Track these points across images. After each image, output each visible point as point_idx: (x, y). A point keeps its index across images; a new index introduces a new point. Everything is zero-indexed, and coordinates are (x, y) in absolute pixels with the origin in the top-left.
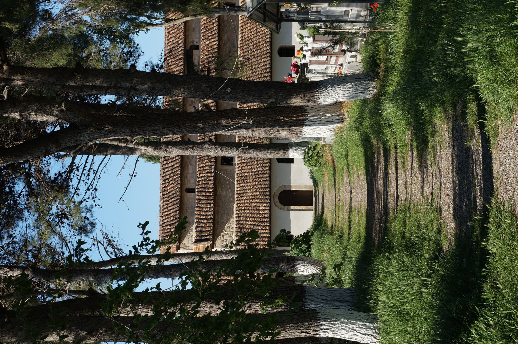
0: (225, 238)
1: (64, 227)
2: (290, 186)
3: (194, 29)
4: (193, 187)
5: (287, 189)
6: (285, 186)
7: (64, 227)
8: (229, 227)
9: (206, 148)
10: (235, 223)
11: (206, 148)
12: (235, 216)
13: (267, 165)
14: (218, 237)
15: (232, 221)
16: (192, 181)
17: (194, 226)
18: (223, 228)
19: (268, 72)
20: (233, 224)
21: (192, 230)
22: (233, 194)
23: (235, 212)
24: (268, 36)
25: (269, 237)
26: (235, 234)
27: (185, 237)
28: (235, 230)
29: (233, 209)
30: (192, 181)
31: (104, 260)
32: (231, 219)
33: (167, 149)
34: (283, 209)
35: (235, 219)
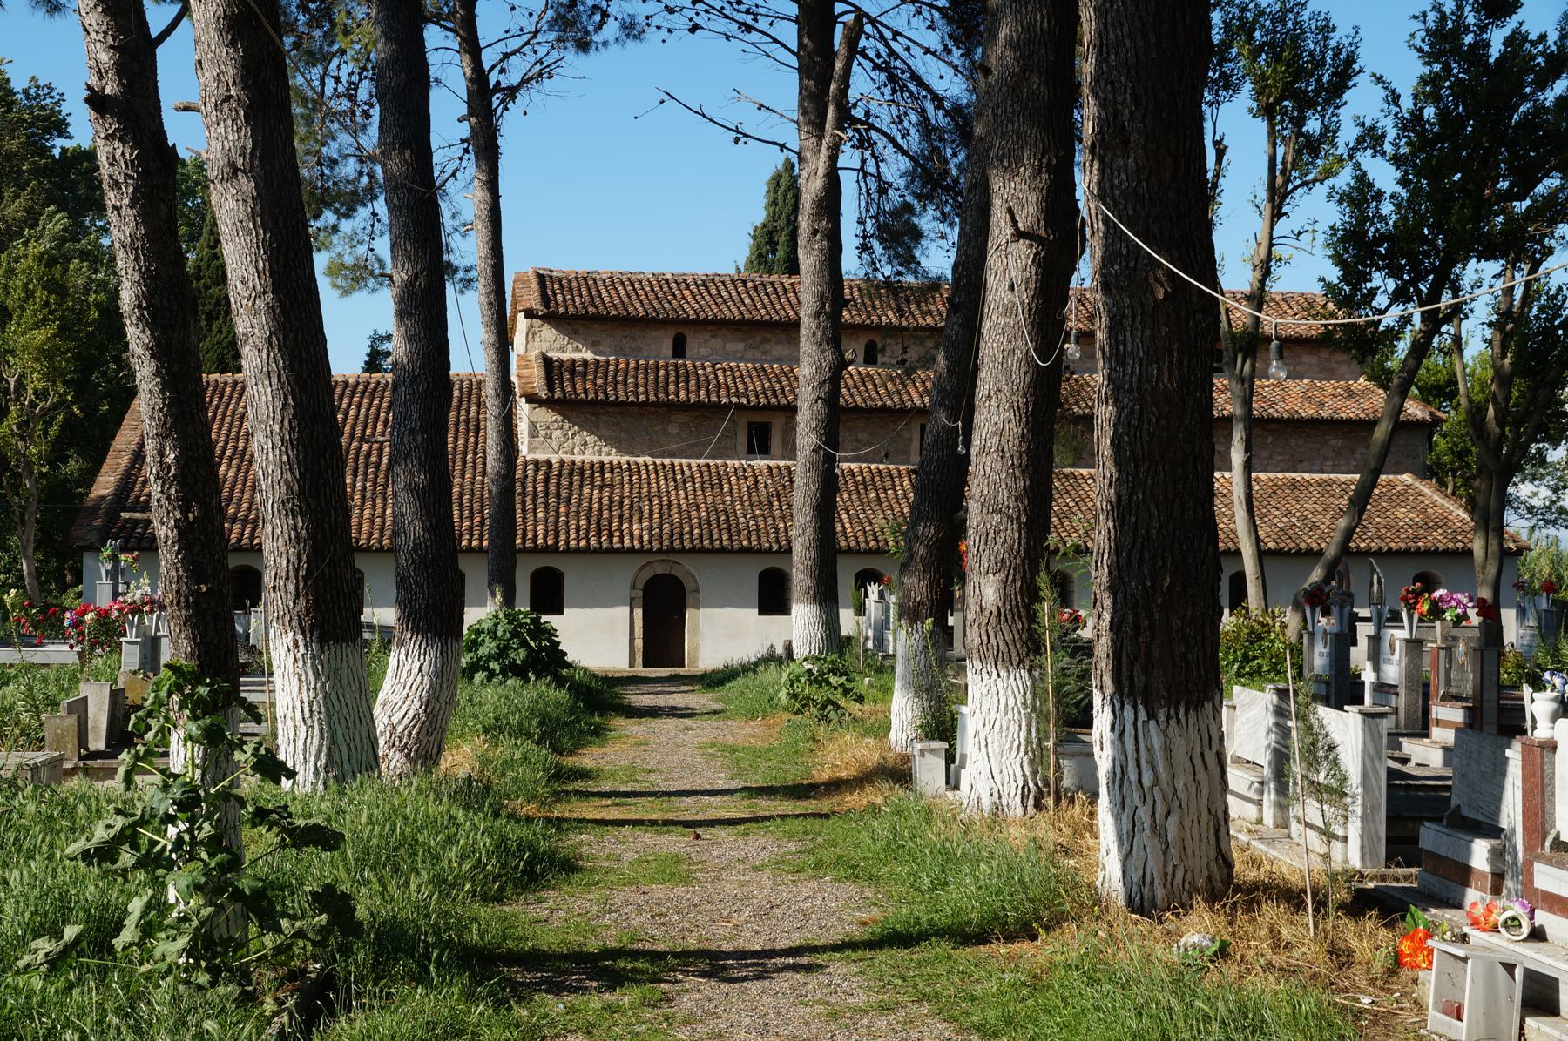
0: (556, 434)
2: (697, 607)
4: (688, 355)
5: (689, 598)
6: (697, 591)
8: (585, 444)
9: (823, 352)
11: (823, 352)
16: (703, 352)
18: (582, 428)
20: (593, 453)
21: (577, 349)
23: (624, 459)
28: (578, 458)
32: (606, 449)
34: (633, 587)
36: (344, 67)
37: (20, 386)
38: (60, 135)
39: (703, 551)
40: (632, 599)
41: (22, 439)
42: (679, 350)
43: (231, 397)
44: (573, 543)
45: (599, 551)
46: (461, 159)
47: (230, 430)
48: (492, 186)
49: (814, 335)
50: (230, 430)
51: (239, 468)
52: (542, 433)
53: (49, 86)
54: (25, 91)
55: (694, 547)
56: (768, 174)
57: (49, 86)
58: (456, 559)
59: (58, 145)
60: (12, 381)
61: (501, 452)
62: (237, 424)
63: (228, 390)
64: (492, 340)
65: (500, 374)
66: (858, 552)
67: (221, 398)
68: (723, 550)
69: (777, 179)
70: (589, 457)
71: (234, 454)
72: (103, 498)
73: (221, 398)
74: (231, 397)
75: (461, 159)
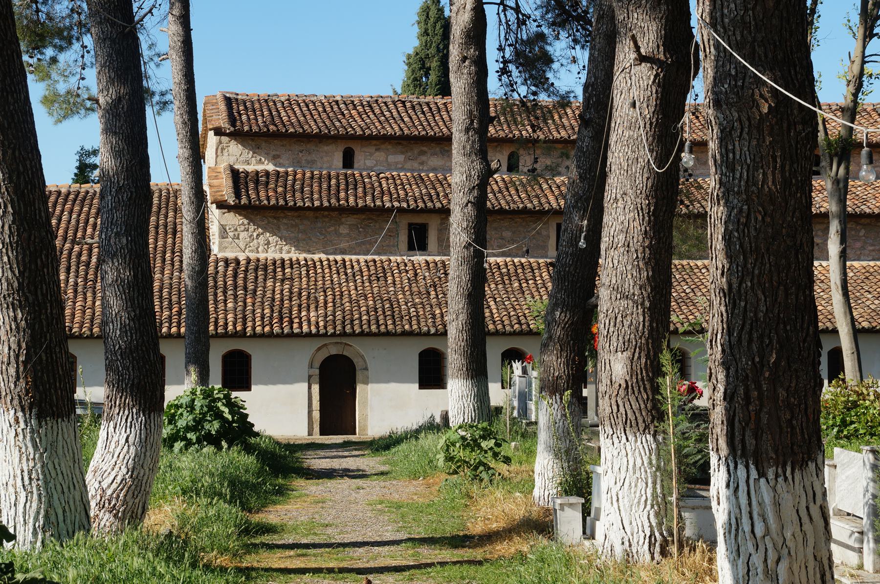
0: (243, 235)
2: (366, 382)
4: (356, 165)
5: (359, 375)
6: (366, 369)
8: (268, 243)
9: (472, 162)
11: (472, 162)
12: (294, 255)
14: (246, 217)
18: (265, 229)
20: (275, 251)
23: (302, 256)
25: (246, 333)
28: (262, 256)
32: (286, 248)
33: (467, 63)
34: (311, 366)
39: (370, 334)
40: (310, 377)
49: (464, 148)
52: (231, 234)
55: (363, 331)
64: (186, 155)
65: (193, 184)
70: (272, 254)
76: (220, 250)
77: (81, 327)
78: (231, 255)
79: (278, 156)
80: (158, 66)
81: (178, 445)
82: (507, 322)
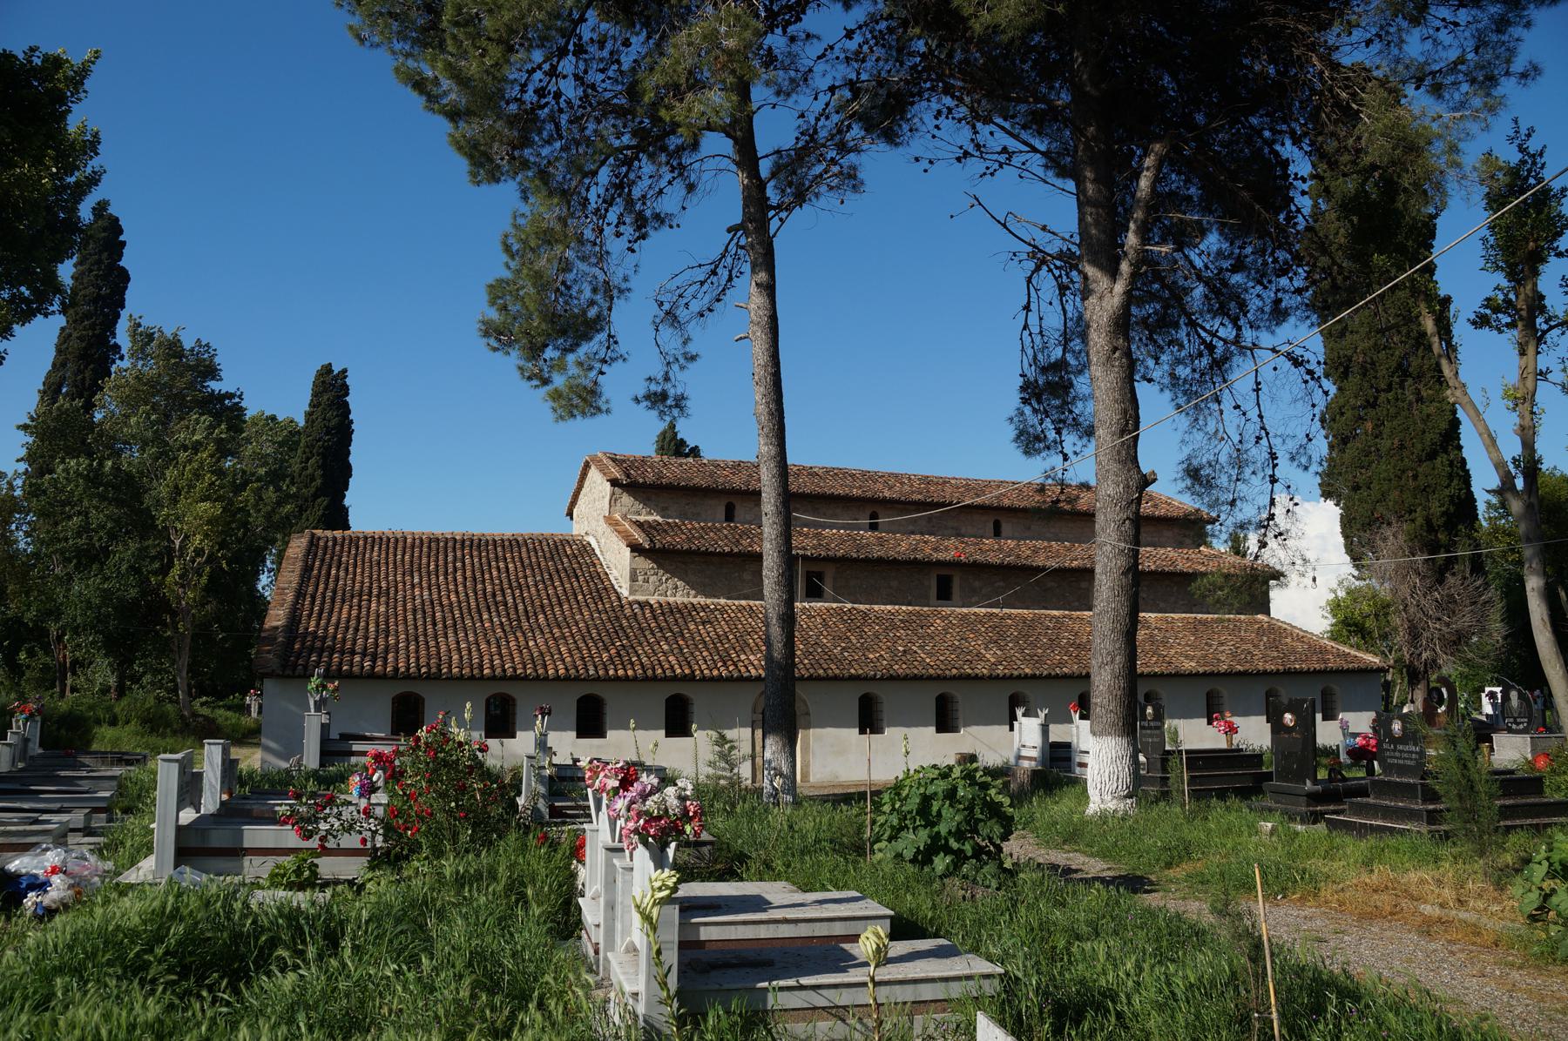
0: (652, 579)
1: (816, 99)
2: (808, 727)
3: (1029, 528)
4: (736, 519)
5: (800, 720)
6: (808, 714)
7: (816, 99)
8: (676, 588)
9: (1129, 471)
10: (686, 600)
11: (1129, 471)
12: (702, 600)
13: (591, 672)
14: (654, 561)
15: (688, 594)
16: (748, 517)
17: (659, 518)
18: (673, 575)
19: (515, 670)
20: (683, 596)
21: (650, 513)
22: (745, 598)
23: (709, 601)
24: (630, 673)
25: (441, 675)
26: (662, 599)
27: (636, 499)
28: (671, 600)
29: (715, 597)
30: (748, 517)
31: (761, 162)
32: (693, 592)
33: (1117, 355)
34: (754, 711)
35: (695, 601)
36: (593, 189)
37: (183, 547)
38: (213, 379)
39: (526, 678)
40: (753, 722)
41: (183, 586)
42: (729, 517)
43: (365, 548)
44: (455, 670)
45: (730, 679)
46: (702, 283)
47: (371, 573)
48: (769, 289)
49: (1119, 453)
50: (371, 573)
51: (387, 604)
52: (640, 578)
53: (207, 345)
54: (192, 350)
55: (538, 676)
56: (658, 432)
57: (207, 345)
58: (794, 686)
59: (214, 385)
60: (177, 543)
61: (782, 575)
62: (375, 568)
63: (361, 543)
64: (773, 453)
65: (781, 490)
66: (577, 679)
67: (357, 548)
68: (836, 678)
69: (664, 434)
70: (680, 599)
71: (380, 593)
72: (276, 628)
73: (357, 548)
74: (365, 548)
75: (702, 283)
76: (631, 593)
77: (525, 668)
78: (641, 598)
79: (667, 508)
80: (682, 368)
81: (941, 862)
82: (704, 667)
